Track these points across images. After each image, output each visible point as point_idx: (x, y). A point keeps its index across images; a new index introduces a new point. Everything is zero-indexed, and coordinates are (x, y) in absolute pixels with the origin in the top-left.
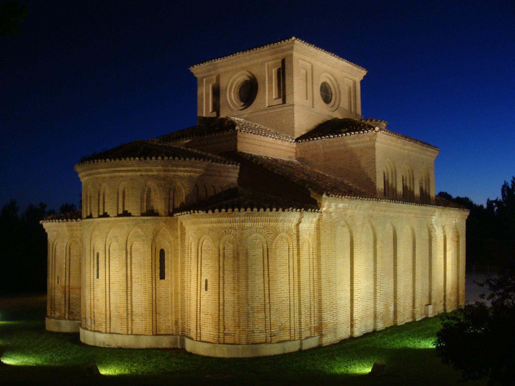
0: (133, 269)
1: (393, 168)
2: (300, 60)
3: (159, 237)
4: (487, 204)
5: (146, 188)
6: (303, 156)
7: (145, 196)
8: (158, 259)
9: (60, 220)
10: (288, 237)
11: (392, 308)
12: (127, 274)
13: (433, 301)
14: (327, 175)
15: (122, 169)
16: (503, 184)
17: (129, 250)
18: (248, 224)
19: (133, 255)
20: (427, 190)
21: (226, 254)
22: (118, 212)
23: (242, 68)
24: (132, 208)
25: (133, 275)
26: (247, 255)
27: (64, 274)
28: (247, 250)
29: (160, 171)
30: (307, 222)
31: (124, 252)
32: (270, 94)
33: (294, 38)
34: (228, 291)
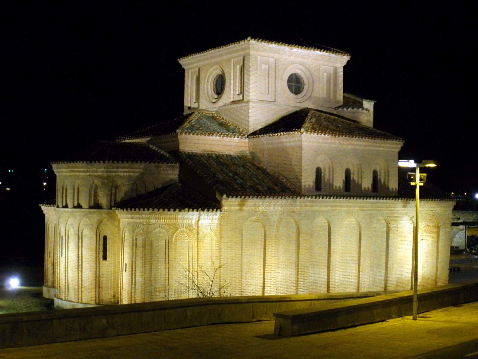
0: (83, 251)
1: (331, 165)
2: (258, 57)
3: (102, 225)
5: (94, 185)
6: (254, 151)
7: (93, 192)
8: (102, 243)
9: (49, 205)
10: (188, 231)
12: (78, 254)
15: (76, 169)
17: (80, 235)
18: (153, 221)
19: (83, 240)
20: (386, 181)
21: (138, 244)
22: (74, 204)
23: (216, 63)
24: (84, 203)
25: (83, 256)
26: (151, 245)
27: (53, 251)
28: (152, 241)
29: (103, 172)
30: (207, 221)
31: (77, 237)
32: (234, 90)
33: (249, 38)
34: (138, 274)
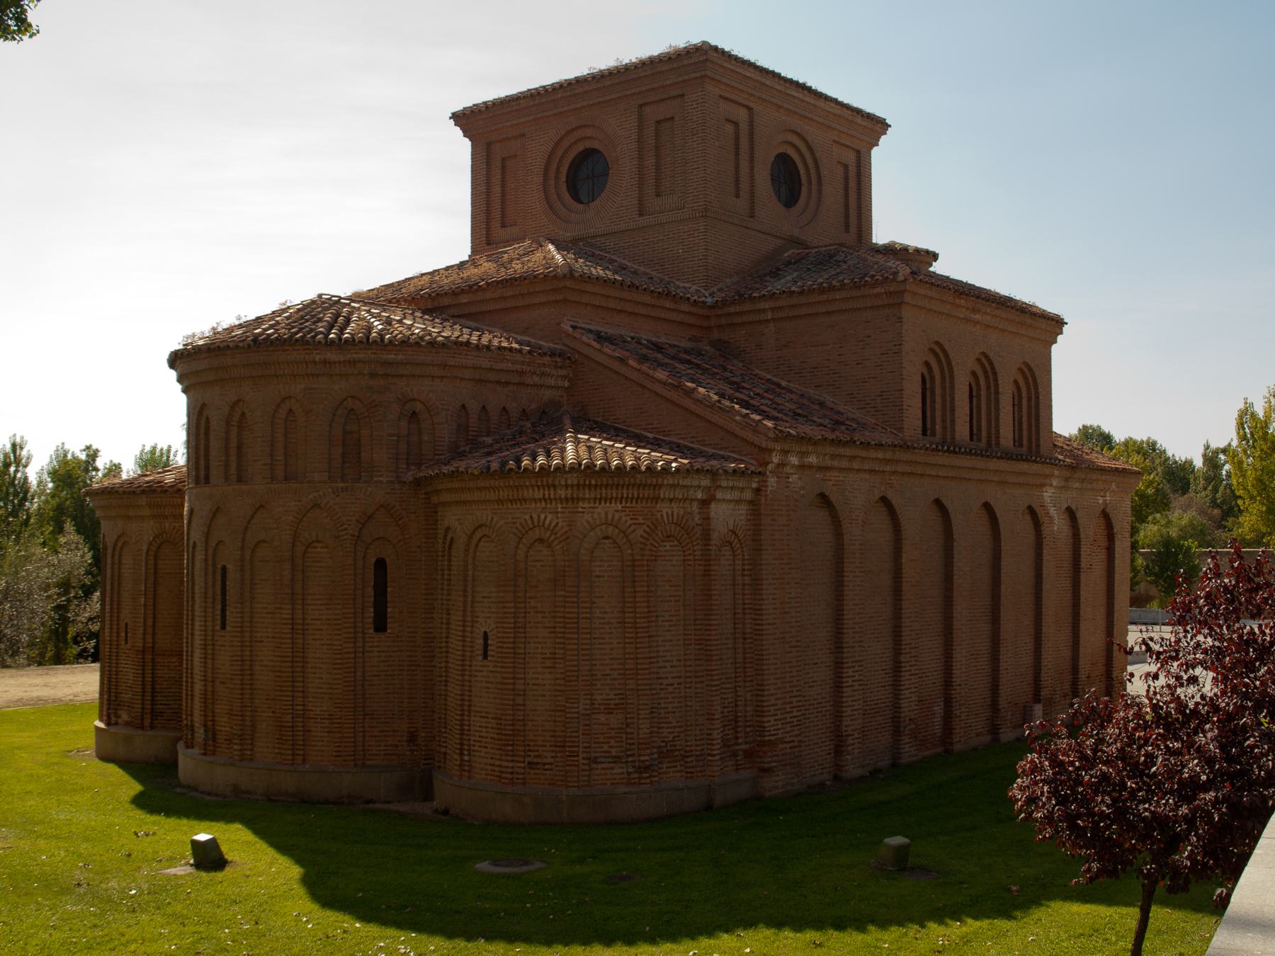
4: (1204, 456)
11: (938, 709)
13: (1045, 693)
16: (1242, 406)
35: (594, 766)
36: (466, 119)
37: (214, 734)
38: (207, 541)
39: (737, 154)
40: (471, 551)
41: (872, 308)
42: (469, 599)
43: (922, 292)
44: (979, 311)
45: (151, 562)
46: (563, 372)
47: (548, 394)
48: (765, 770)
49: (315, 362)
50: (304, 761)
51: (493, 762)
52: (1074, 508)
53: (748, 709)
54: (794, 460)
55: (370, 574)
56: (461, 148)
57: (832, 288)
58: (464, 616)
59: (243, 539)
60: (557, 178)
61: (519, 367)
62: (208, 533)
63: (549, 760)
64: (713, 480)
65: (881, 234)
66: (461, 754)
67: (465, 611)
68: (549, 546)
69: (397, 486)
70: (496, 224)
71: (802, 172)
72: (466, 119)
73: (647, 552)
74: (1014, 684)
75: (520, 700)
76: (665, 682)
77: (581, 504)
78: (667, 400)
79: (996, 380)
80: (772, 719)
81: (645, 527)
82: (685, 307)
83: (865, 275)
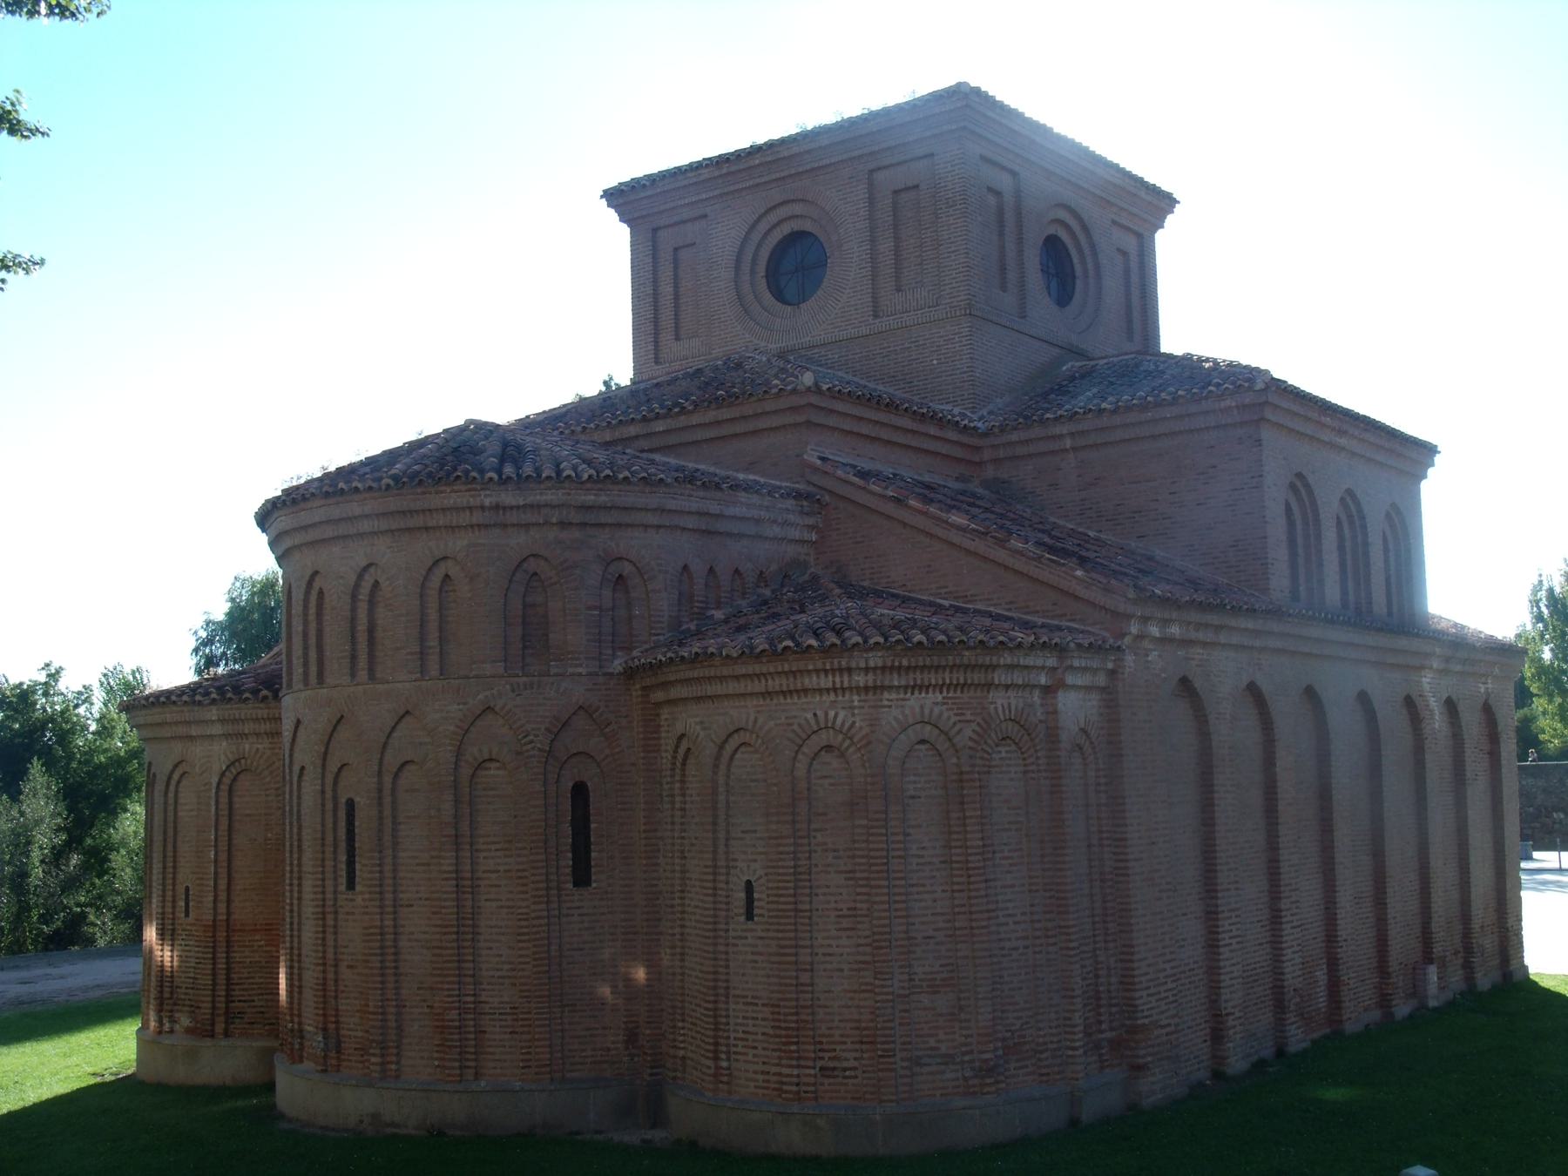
11: (1321, 975)
13: (1437, 949)
14: (1091, 534)
35: (917, 1069)
36: (623, 198)
37: (339, 1043)
38: (324, 766)
39: (1001, 234)
40: (723, 767)
41: (1217, 427)
42: (722, 835)
43: (1285, 404)
44: (1345, 432)
45: (224, 800)
46: (811, 521)
47: (791, 551)
48: (1139, 1068)
49: (483, 508)
50: (477, 1076)
51: (766, 1068)
52: (1454, 698)
53: (1113, 980)
54: (1155, 631)
55: (567, 805)
56: (616, 238)
57: (1159, 404)
58: (714, 859)
59: (381, 760)
60: (753, 272)
61: (755, 513)
62: (326, 753)
63: (852, 1063)
64: (1061, 658)
65: (1173, 340)
66: (716, 1059)
67: (715, 852)
68: (842, 755)
69: (601, 679)
70: (667, 337)
71: (1076, 260)
72: (623, 198)
73: (979, 762)
74: (1402, 945)
75: (805, 978)
76: (1007, 944)
77: (886, 695)
78: (968, 552)
79: (1364, 527)
80: (1144, 993)
81: (974, 726)
82: (952, 435)
83: (1209, 384)
